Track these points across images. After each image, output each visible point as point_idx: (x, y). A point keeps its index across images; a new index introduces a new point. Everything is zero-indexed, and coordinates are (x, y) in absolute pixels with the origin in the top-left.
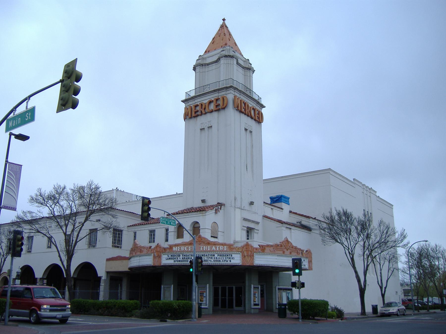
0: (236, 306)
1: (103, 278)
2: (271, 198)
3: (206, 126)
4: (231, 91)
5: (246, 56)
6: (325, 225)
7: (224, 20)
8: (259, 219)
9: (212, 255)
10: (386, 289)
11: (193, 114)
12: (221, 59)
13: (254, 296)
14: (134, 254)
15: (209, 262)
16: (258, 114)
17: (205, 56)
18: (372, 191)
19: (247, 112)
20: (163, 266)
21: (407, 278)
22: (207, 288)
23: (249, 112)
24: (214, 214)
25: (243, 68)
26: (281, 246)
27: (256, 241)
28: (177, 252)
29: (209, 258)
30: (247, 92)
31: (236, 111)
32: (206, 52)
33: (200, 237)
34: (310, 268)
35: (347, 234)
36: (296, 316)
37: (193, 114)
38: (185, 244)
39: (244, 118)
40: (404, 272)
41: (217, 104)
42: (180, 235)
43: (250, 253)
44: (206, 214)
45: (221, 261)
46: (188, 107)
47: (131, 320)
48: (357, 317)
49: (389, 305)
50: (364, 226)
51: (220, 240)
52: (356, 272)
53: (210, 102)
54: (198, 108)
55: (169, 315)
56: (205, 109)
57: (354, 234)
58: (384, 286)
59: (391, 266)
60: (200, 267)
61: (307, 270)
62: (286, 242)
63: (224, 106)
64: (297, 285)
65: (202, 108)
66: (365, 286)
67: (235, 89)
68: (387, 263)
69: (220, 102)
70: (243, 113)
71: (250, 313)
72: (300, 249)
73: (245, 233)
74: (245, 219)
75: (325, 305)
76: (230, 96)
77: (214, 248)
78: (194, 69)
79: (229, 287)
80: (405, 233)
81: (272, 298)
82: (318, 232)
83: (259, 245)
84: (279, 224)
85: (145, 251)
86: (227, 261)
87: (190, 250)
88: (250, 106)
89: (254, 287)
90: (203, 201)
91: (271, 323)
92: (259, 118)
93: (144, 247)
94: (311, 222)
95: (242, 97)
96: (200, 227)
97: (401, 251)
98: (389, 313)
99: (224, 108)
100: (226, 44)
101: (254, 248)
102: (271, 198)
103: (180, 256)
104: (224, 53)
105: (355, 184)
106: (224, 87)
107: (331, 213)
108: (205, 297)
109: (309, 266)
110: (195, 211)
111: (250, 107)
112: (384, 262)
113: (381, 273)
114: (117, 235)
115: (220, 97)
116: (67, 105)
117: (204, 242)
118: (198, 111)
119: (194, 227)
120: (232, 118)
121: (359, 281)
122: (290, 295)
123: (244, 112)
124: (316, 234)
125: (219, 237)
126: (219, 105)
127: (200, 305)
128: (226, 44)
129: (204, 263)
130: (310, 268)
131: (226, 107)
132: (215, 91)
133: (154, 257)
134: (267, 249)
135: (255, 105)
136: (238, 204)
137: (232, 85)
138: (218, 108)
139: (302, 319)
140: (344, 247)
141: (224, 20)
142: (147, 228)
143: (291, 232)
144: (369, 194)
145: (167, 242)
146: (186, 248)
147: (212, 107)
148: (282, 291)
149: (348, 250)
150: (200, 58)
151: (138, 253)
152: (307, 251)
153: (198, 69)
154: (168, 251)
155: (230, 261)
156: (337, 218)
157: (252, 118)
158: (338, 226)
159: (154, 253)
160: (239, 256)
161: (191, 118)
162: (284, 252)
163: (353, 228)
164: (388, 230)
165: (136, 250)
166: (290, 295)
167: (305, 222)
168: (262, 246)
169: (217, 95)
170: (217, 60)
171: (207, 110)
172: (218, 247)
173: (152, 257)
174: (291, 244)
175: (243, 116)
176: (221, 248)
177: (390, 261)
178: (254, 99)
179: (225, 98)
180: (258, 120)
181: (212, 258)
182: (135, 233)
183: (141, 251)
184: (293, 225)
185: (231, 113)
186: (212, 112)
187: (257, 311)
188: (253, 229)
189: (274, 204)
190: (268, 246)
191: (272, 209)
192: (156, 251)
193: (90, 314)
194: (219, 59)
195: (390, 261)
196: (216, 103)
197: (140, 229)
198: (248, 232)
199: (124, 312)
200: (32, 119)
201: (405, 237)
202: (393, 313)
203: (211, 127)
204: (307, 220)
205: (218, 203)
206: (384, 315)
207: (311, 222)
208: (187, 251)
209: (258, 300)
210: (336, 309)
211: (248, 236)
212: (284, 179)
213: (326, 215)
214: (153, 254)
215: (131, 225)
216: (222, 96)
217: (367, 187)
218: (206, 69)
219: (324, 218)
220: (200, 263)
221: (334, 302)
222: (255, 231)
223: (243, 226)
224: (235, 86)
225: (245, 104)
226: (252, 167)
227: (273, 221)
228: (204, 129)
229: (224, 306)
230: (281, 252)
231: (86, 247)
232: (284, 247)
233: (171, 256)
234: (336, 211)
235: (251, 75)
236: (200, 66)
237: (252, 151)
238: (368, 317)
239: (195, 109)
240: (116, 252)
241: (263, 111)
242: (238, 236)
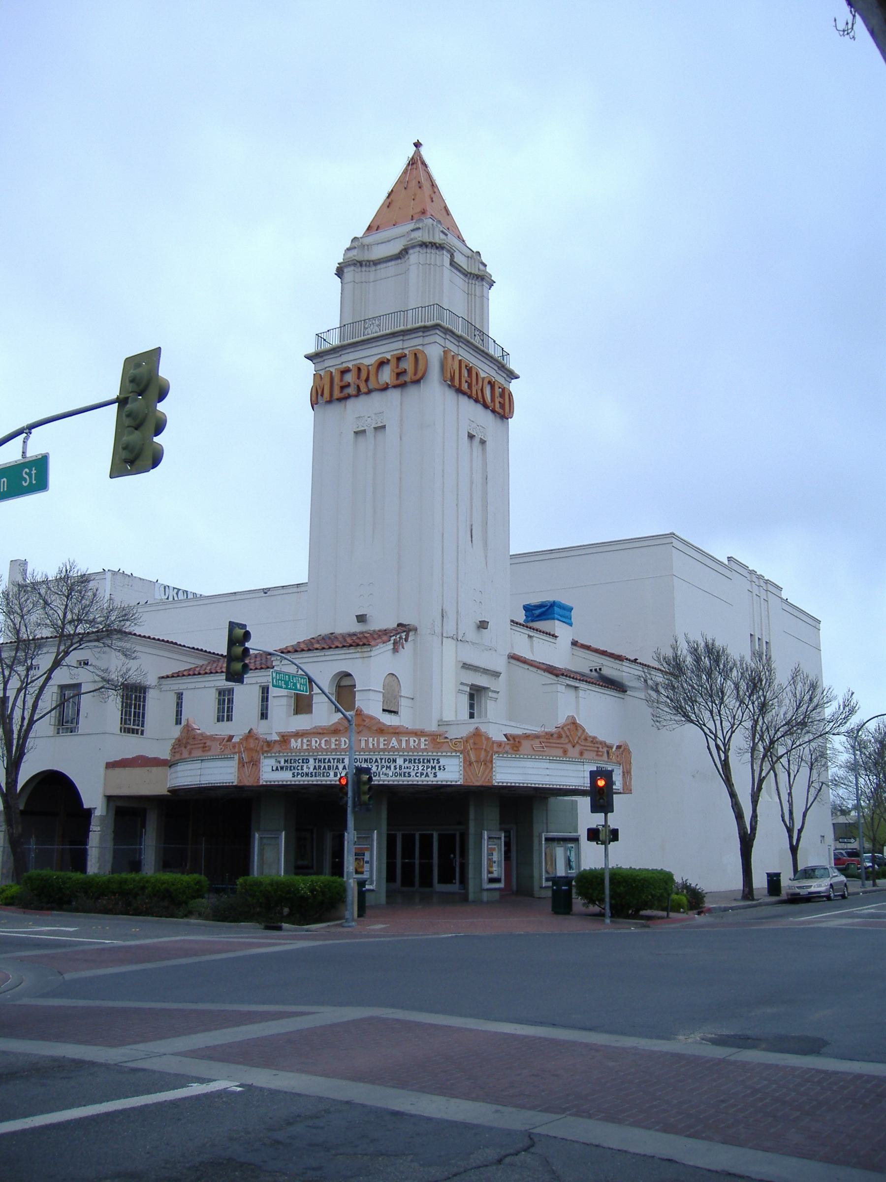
0: (439, 882)
1: (98, 813)
2: (528, 609)
3: (369, 424)
4: (437, 337)
5: (473, 242)
6: (659, 678)
7: (417, 145)
8: (499, 663)
9: (389, 760)
10: (802, 834)
11: (337, 393)
12: (411, 251)
13: (489, 857)
14: (185, 754)
15: (383, 777)
16: (502, 395)
17: (367, 241)
18: (771, 588)
19: (474, 392)
20: (263, 786)
21: (844, 795)
22: (373, 840)
23: (479, 392)
24: (390, 653)
25: (466, 274)
26: (560, 736)
27: (497, 724)
28: (300, 751)
29: (383, 767)
30: (475, 339)
31: (447, 389)
32: (369, 228)
33: (359, 713)
34: (627, 790)
35: (713, 702)
36: (595, 909)
37: (337, 393)
38: (319, 732)
39: (468, 408)
40: (845, 786)
41: (399, 370)
42: (302, 705)
43: (483, 754)
44: (372, 653)
45: (413, 774)
46: (322, 373)
47: (188, 924)
48: (734, 904)
49: (809, 873)
50: (756, 683)
51: (404, 720)
52: (733, 795)
53: (382, 364)
54: (349, 378)
55: (286, 910)
56: (367, 380)
57: (731, 701)
58: (797, 826)
59: (815, 776)
60: (365, 793)
61: (620, 793)
62: (572, 727)
63: (418, 377)
64: (602, 836)
65: (359, 378)
66: (754, 829)
67: (448, 331)
68: (805, 770)
69: (407, 365)
70: (464, 393)
71: (479, 902)
72: (603, 744)
73: (465, 700)
74: (466, 666)
75: (666, 883)
76: (434, 350)
77: (394, 742)
78: (340, 272)
79: (421, 835)
80: (854, 701)
81: (531, 864)
82: (642, 695)
83: (505, 735)
84: (549, 678)
85: (216, 748)
86: (427, 775)
87: (333, 746)
88: (482, 375)
89: (489, 838)
90: (361, 619)
91: (534, 925)
92: (502, 406)
93: (212, 738)
94: (624, 669)
95: (462, 352)
96: (354, 686)
97: (839, 744)
98: (810, 893)
99: (417, 382)
100: (424, 212)
101: (493, 742)
102: (528, 609)
103: (308, 761)
104: (419, 236)
105: (731, 569)
106: (417, 325)
107: (675, 648)
108: (367, 862)
109: (625, 784)
110: (344, 646)
111: (483, 379)
112: (799, 766)
113: (790, 794)
114: (133, 697)
115: (406, 351)
116: (137, 462)
117: (369, 728)
118: (348, 385)
119: (339, 687)
120: (437, 408)
121: (739, 816)
122: (573, 853)
123: (468, 391)
124: (636, 700)
125: (403, 711)
126: (405, 372)
127: (361, 884)
128: (424, 212)
129: (376, 781)
130: (627, 790)
131: (422, 378)
132: (393, 335)
133: (242, 764)
134: (526, 745)
135: (493, 373)
136: (450, 629)
137: (438, 321)
138: (402, 379)
139: (612, 916)
140: (705, 734)
141: (417, 145)
142: (212, 684)
143: (577, 697)
144: (763, 595)
145: (264, 721)
146: (323, 741)
147: (386, 375)
148: (555, 844)
149: (715, 740)
150: (356, 244)
151: (197, 753)
152: (619, 747)
153: (349, 273)
154: (277, 748)
155: (435, 776)
156: (689, 660)
157: (486, 406)
158: (693, 681)
159: (240, 752)
160: (456, 761)
161: (330, 402)
162: (565, 752)
163: (729, 686)
164: (812, 692)
165: (190, 743)
166: (573, 853)
167: (611, 669)
168: (514, 737)
169: (399, 345)
170: (401, 253)
171: (372, 384)
172: (404, 739)
173: (234, 763)
174: (584, 730)
175: (464, 401)
176: (412, 743)
177: (812, 765)
178: (491, 357)
179: (420, 356)
180: (501, 411)
181: (390, 767)
182: (180, 696)
183: (205, 748)
184: (582, 678)
185: (434, 395)
186: (385, 388)
187: (497, 895)
188: (485, 689)
189: (536, 625)
190: (527, 737)
191: (530, 637)
192: (246, 749)
193: (77, 910)
194: (404, 252)
195: (812, 765)
196: (398, 367)
197: (192, 686)
198: (471, 697)
199: (167, 904)
200: (41, 484)
201: (852, 711)
202: (819, 892)
203: (384, 427)
204: (616, 664)
205: (399, 625)
206: (795, 899)
207: (624, 669)
208: (327, 750)
209: (498, 871)
210: (686, 887)
211: (472, 706)
212: (557, 555)
213: (663, 653)
214: (236, 757)
215: (170, 673)
216: (409, 345)
217: (760, 577)
218: (372, 274)
219: (659, 661)
220: (365, 783)
221: (686, 871)
222: (490, 694)
223: (462, 684)
224: (445, 324)
225: (470, 371)
226: (485, 531)
227: (535, 670)
228: (364, 431)
229: (408, 881)
230: (559, 752)
231: (51, 731)
232: (568, 739)
233: (286, 761)
234: (688, 642)
235: (485, 295)
236: (355, 265)
237: (485, 494)
238: (760, 905)
239: (341, 380)
240: (132, 746)
241: (514, 387)
242: (448, 708)
